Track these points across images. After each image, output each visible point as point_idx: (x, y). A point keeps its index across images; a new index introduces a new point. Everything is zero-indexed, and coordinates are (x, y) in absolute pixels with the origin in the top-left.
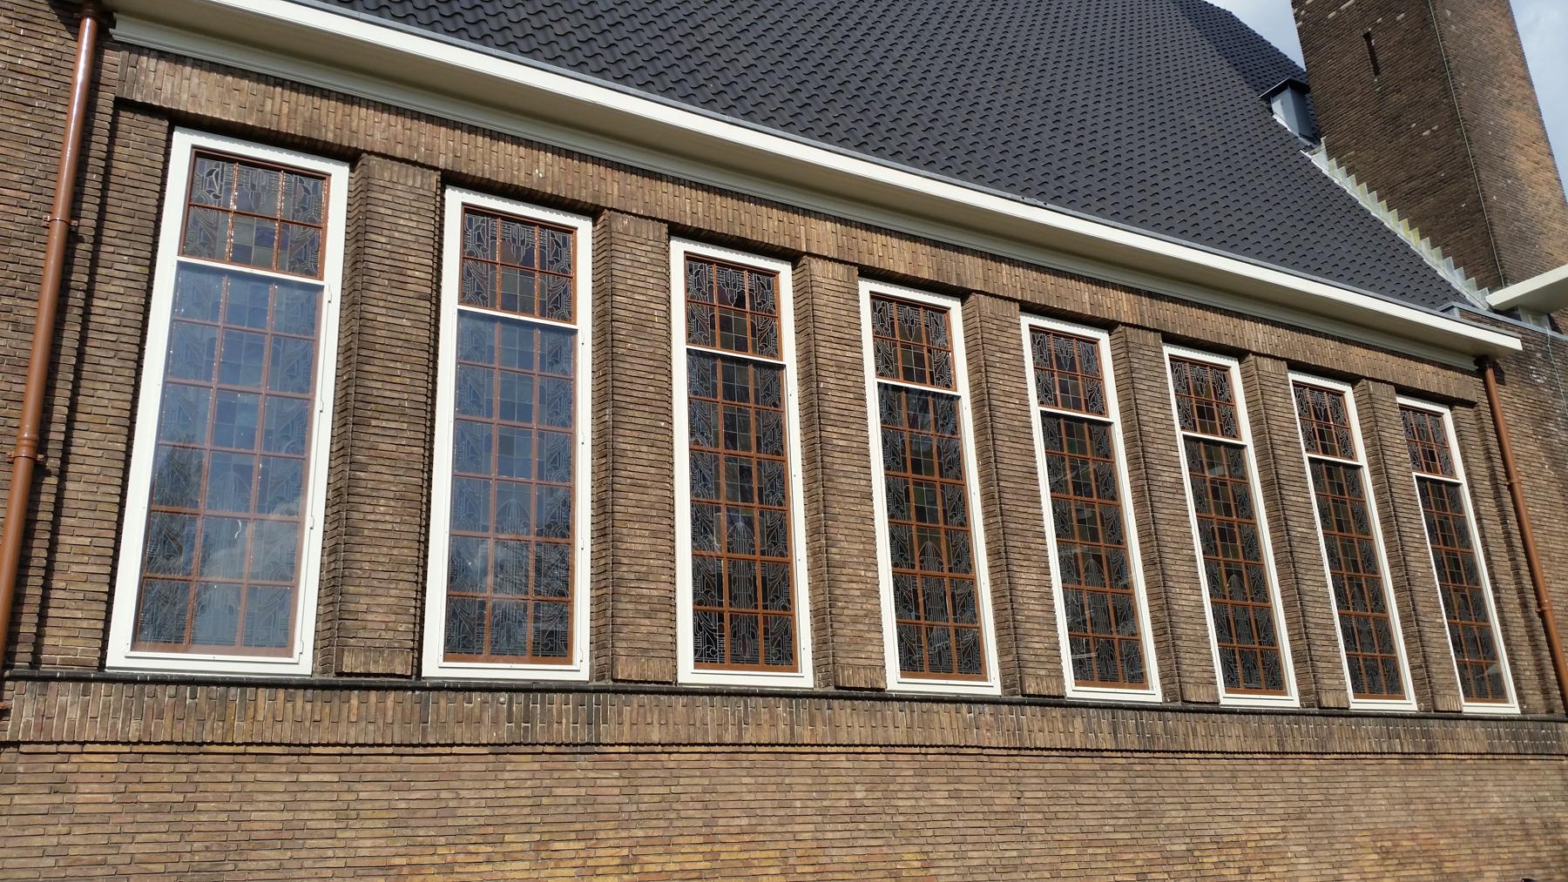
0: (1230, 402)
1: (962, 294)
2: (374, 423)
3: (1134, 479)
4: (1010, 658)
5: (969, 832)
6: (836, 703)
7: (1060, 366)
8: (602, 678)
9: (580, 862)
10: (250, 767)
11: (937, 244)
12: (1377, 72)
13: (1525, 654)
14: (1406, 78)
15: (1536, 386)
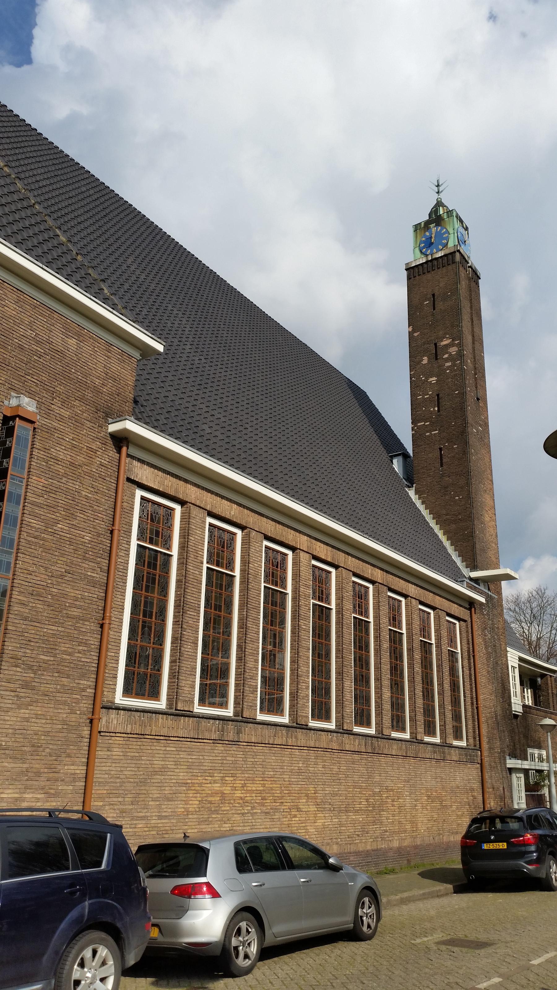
0: (170, 528)
1: (336, 567)
2: (188, 612)
3: (375, 645)
4: (340, 715)
5: (327, 781)
6: (298, 730)
7: (152, 520)
8: (171, 708)
9: (232, 785)
10: (155, 744)
11: (333, 547)
12: (442, 466)
13: (470, 722)
14: (453, 473)
15: (483, 615)
